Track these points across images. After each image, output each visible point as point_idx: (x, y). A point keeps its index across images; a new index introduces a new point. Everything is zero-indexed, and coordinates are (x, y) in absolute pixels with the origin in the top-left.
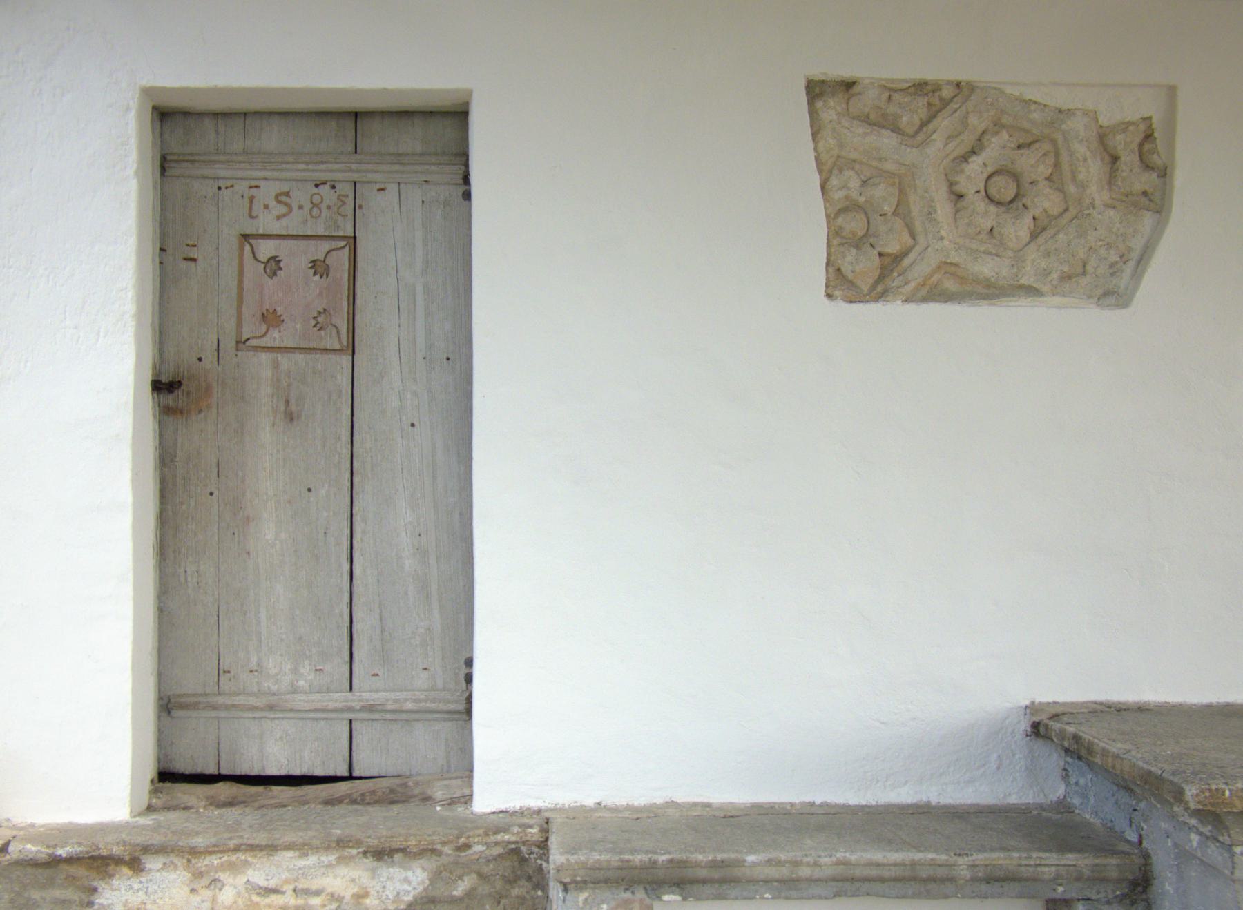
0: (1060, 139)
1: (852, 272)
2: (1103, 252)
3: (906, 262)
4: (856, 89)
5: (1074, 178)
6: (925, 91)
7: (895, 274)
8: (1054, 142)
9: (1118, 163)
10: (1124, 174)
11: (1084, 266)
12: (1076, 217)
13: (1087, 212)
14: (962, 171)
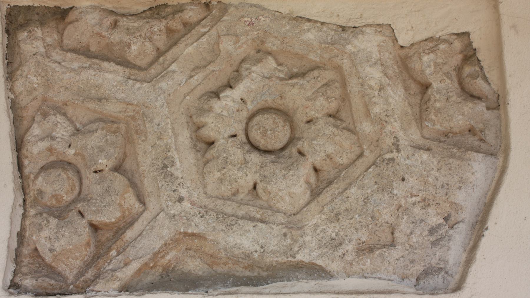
0: (346, 64)
1: (51, 250)
2: (417, 210)
3: (129, 234)
4: (71, 16)
5: (368, 113)
6: (163, 14)
7: (113, 253)
8: (338, 69)
9: (430, 91)
10: (438, 105)
11: (393, 233)
12: (374, 164)
13: (388, 156)
14: (210, 110)
